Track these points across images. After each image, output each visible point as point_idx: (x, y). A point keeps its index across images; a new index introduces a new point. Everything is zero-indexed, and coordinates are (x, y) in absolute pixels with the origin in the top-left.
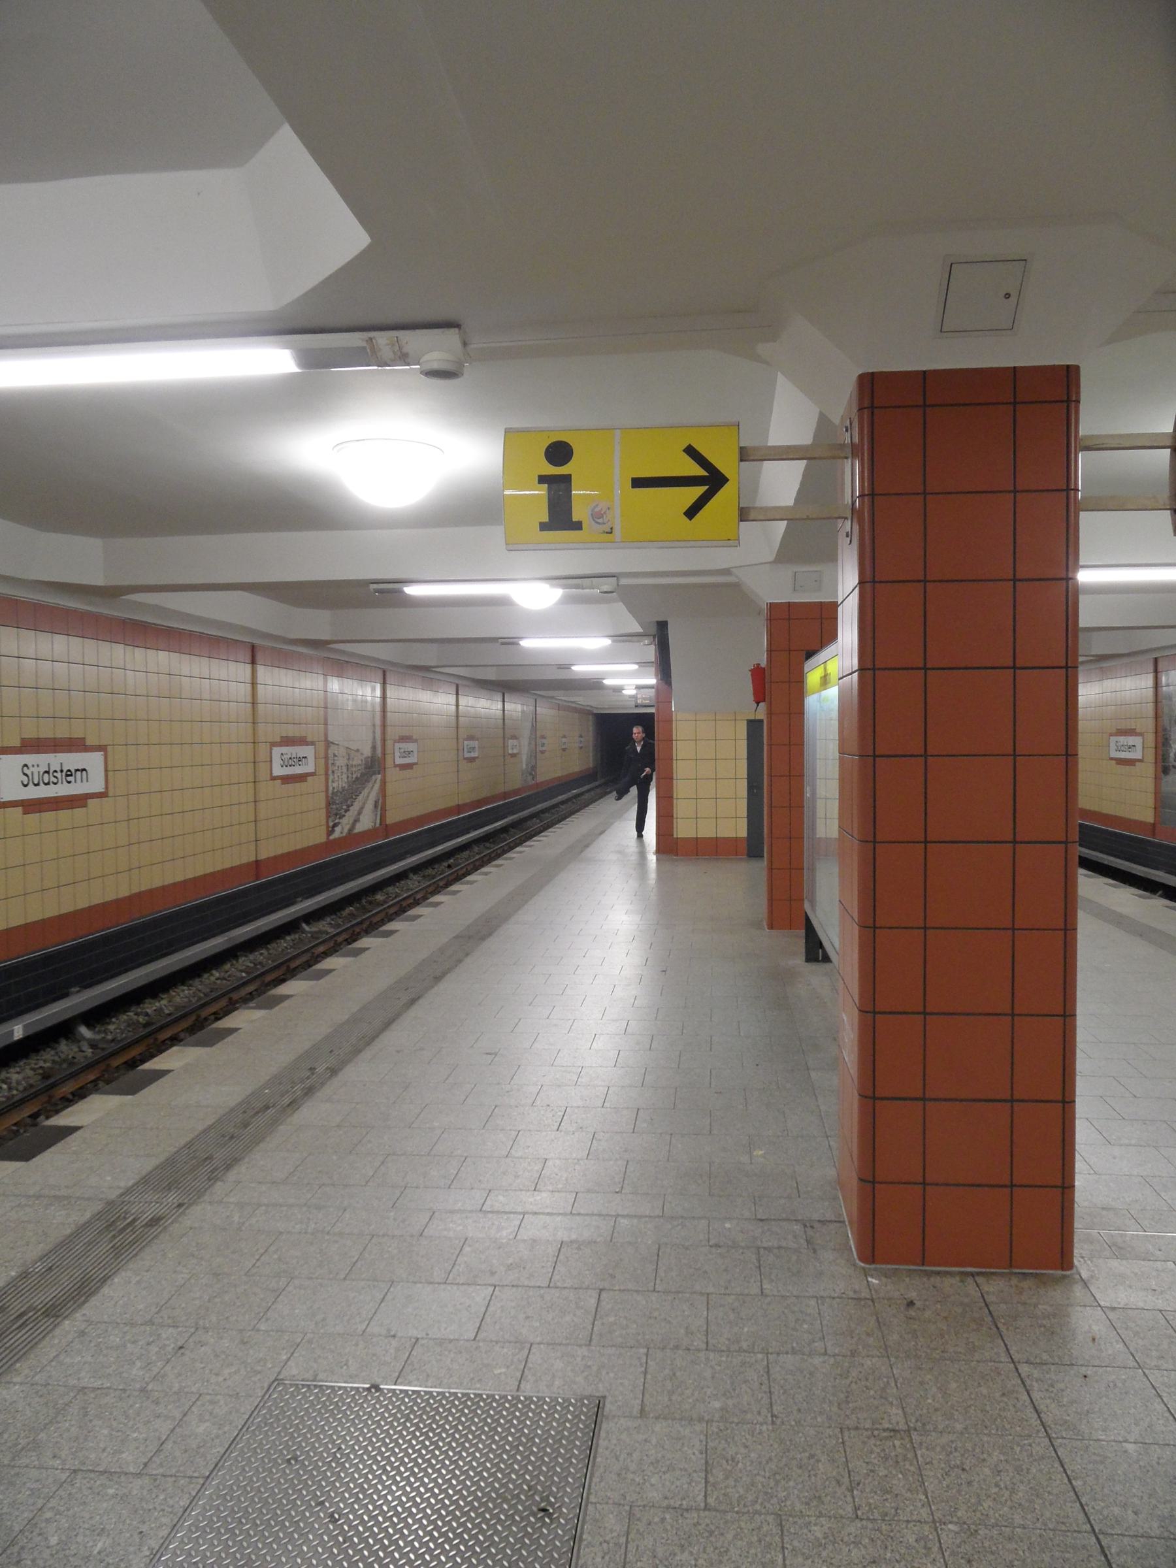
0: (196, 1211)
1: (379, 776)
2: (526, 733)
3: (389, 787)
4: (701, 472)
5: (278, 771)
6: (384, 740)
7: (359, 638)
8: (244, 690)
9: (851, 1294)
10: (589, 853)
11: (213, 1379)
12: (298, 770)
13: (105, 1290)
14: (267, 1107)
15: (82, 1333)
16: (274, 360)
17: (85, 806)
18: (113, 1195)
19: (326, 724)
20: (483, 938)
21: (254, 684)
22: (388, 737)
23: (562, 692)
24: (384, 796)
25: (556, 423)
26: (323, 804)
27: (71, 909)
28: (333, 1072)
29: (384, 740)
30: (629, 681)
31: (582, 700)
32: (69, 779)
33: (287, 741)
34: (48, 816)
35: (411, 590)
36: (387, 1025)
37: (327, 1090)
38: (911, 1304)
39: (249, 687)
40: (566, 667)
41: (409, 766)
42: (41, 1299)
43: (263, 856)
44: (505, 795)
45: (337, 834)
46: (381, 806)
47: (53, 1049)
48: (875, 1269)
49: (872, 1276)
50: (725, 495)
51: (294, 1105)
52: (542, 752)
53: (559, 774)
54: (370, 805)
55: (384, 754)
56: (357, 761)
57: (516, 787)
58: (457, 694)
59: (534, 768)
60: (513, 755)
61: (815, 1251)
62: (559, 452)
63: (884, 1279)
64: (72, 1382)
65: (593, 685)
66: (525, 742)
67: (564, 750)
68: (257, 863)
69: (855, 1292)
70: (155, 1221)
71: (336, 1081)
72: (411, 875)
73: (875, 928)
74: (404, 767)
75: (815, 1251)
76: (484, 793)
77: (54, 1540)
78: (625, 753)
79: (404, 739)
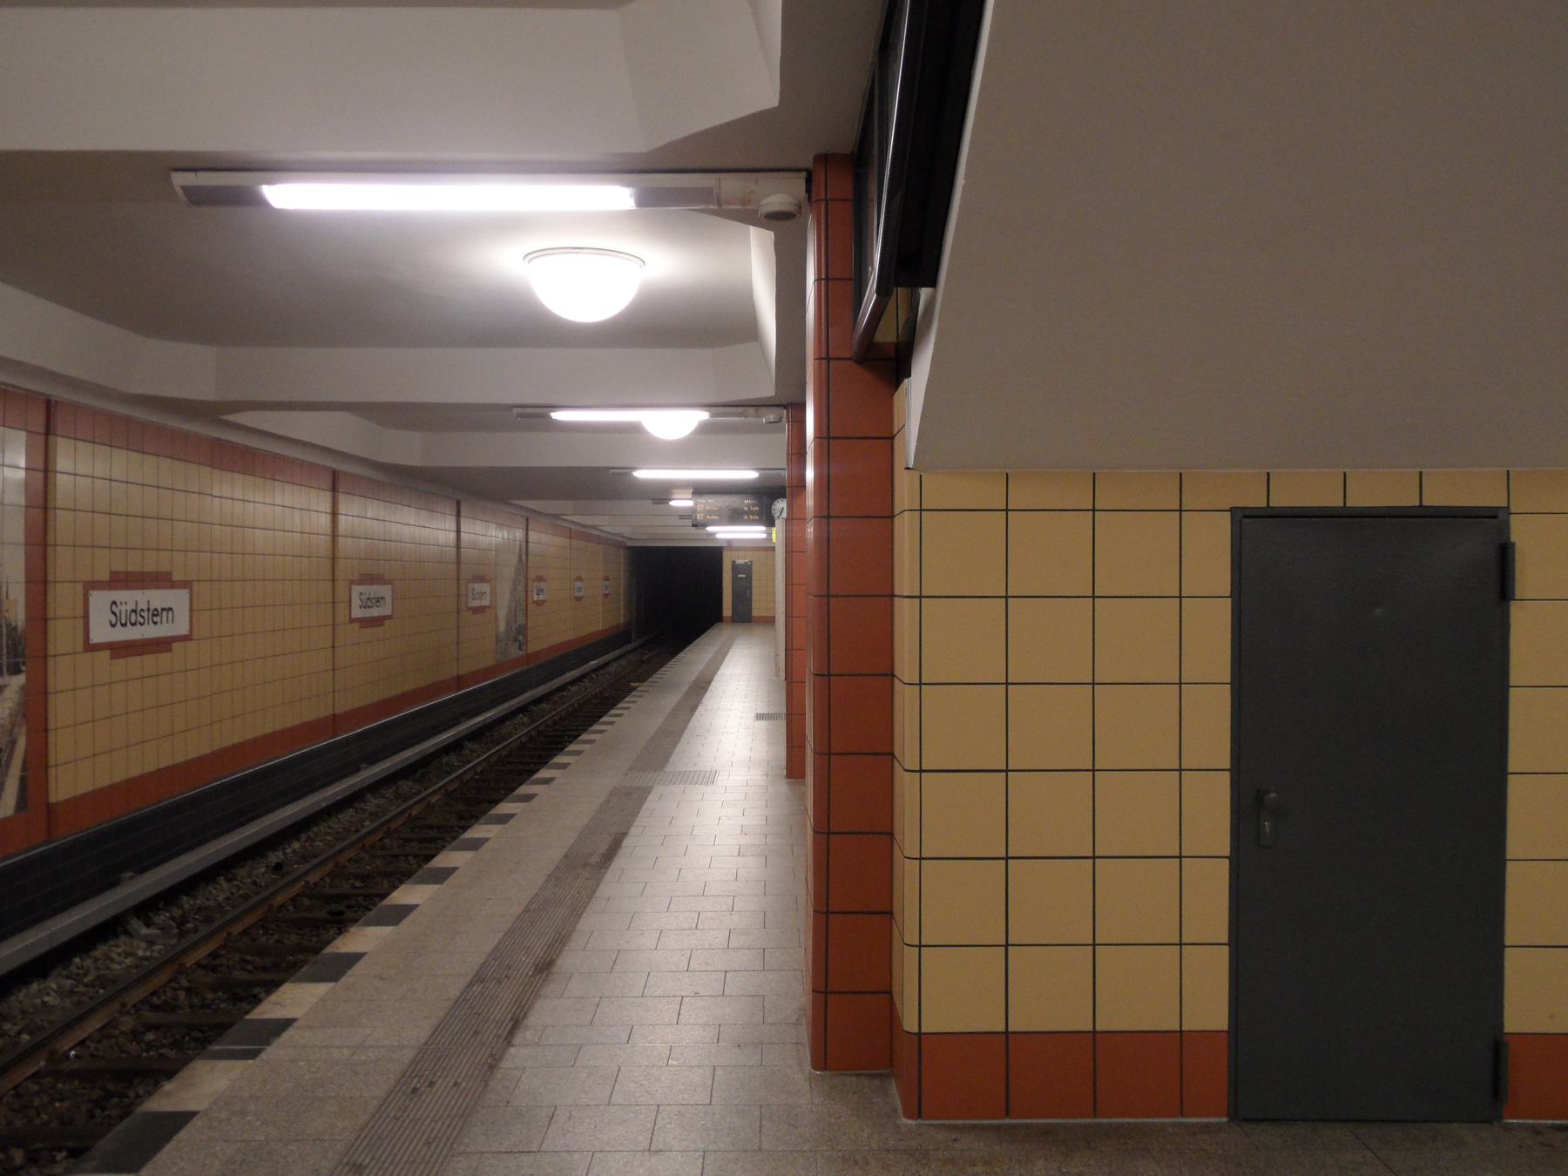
1: (20, 680)
2: (508, 572)
5: (357, 613)
12: (375, 612)
17: (170, 650)
21: (458, 532)
22: (340, 574)
27: (90, 788)
33: (122, 580)
34: (135, 661)
41: (378, 621)
43: (340, 710)
44: (459, 681)
47: (65, 968)
52: (539, 603)
53: (570, 636)
57: (490, 662)
58: (458, 515)
59: (522, 630)
66: (505, 590)
67: (578, 599)
68: (459, 677)
72: (369, 796)
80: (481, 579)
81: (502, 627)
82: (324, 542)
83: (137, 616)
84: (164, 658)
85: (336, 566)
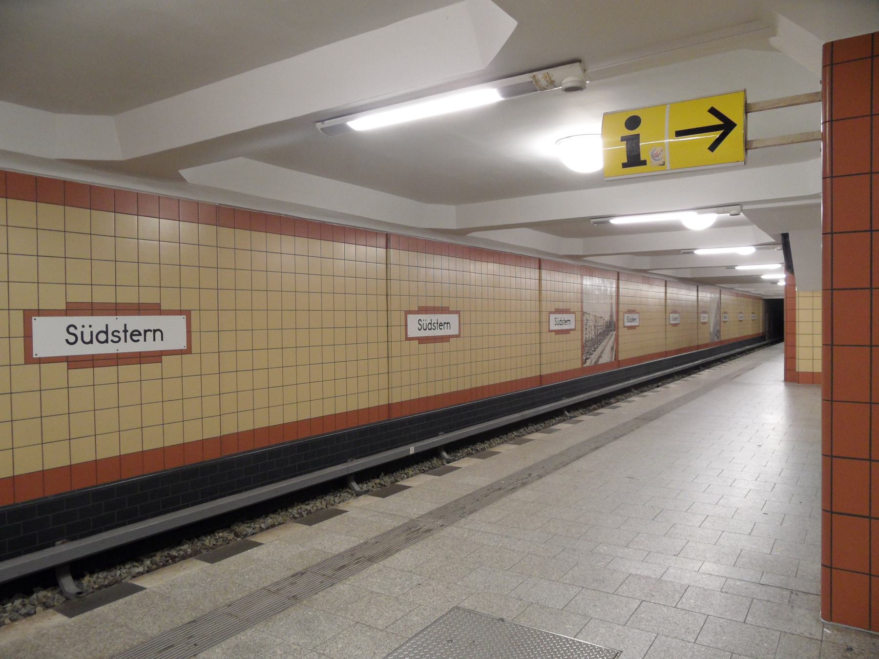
0: (449, 529)
2: (714, 310)
3: (620, 339)
4: (720, 122)
5: (553, 327)
6: (618, 312)
7: (596, 253)
8: (534, 284)
9: (807, 635)
10: (737, 380)
11: (428, 600)
12: (565, 327)
13: (397, 555)
14: (500, 489)
15: (380, 570)
16: (488, 96)
18: (415, 517)
19: (582, 302)
20: (651, 420)
22: (620, 310)
23: (738, 285)
24: (618, 344)
25: (628, 105)
26: (580, 347)
28: (540, 477)
29: (618, 312)
30: (773, 272)
31: (753, 290)
32: (135, 338)
33: (558, 311)
35: (614, 221)
36: (578, 458)
37: (534, 485)
38: (850, 649)
39: (537, 281)
40: (732, 267)
41: (633, 327)
42: (368, 554)
44: (698, 347)
45: (588, 363)
46: (616, 350)
48: (833, 626)
49: (827, 628)
50: (736, 135)
51: (514, 490)
52: (725, 322)
53: (737, 336)
54: (608, 348)
55: (618, 320)
56: (601, 323)
58: (618, 279)
59: (719, 331)
60: (704, 323)
61: (792, 607)
62: (633, 122)
63: (835, 632)
64: (369, 588)
65: (753, 279)
66: (713, 315)
69: (811, 634)
70: (429, 531)
71: (540, 481)
72: (444, 454)
73: (832, 401)
74: (630, 328)
75: (792, 607)
76: (684, 345)
77: (340, 646)
78: (774, 323)
79: (630, 312)
80: (705, 312)
81: (712, 330)
82: (663, 301)
83: (431, 326)
84: (446, 345)
85: (667, 308)
